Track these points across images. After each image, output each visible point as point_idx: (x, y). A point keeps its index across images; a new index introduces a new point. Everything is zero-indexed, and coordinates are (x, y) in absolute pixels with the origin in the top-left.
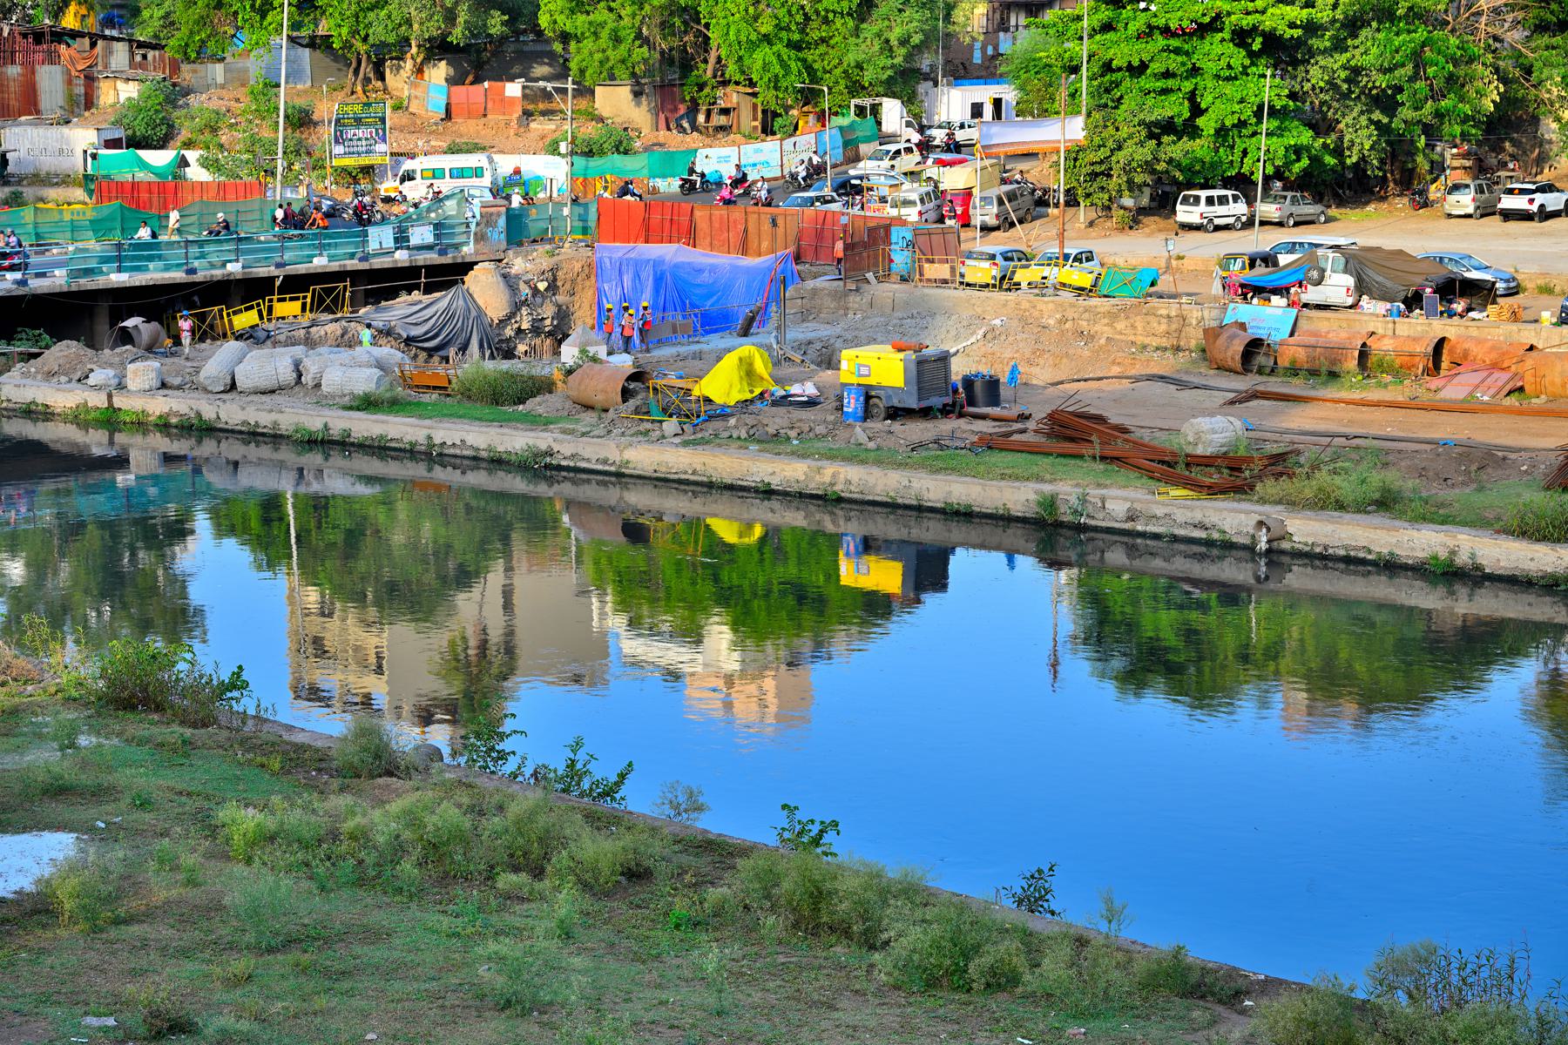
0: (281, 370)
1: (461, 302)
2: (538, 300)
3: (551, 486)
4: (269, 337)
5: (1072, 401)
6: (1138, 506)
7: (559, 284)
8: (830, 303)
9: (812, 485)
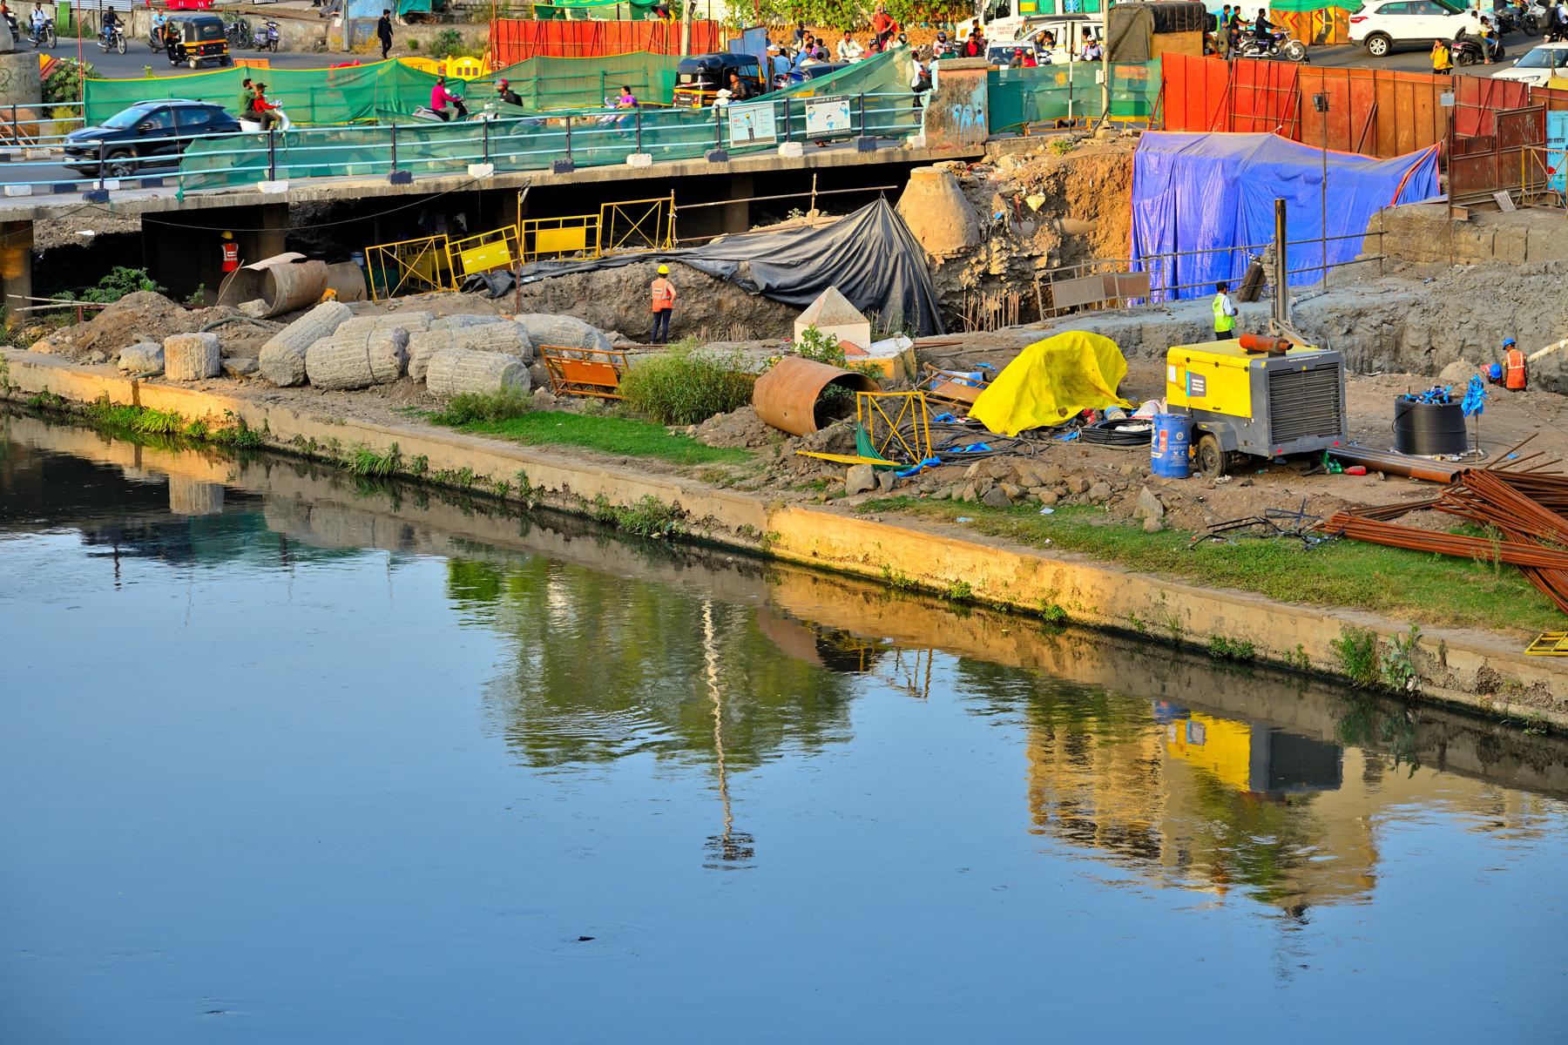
0: (375, 352)
1: (878, 229)
2: (1027, 225)
3: (678, 569)
4: (512, 286)
5: (1525, 452)
6: (1494, 665)
7: (1070, 198)
8: (1429, 243)
9: (1026, 594)
